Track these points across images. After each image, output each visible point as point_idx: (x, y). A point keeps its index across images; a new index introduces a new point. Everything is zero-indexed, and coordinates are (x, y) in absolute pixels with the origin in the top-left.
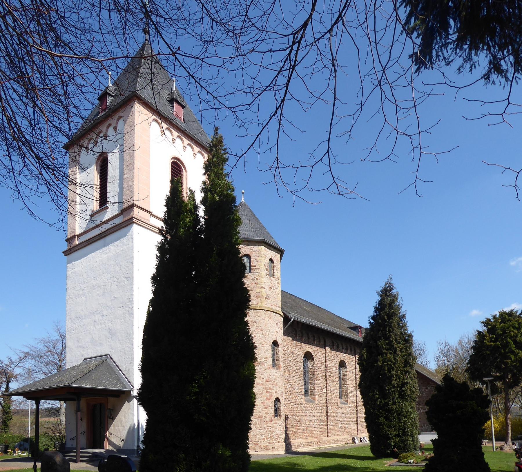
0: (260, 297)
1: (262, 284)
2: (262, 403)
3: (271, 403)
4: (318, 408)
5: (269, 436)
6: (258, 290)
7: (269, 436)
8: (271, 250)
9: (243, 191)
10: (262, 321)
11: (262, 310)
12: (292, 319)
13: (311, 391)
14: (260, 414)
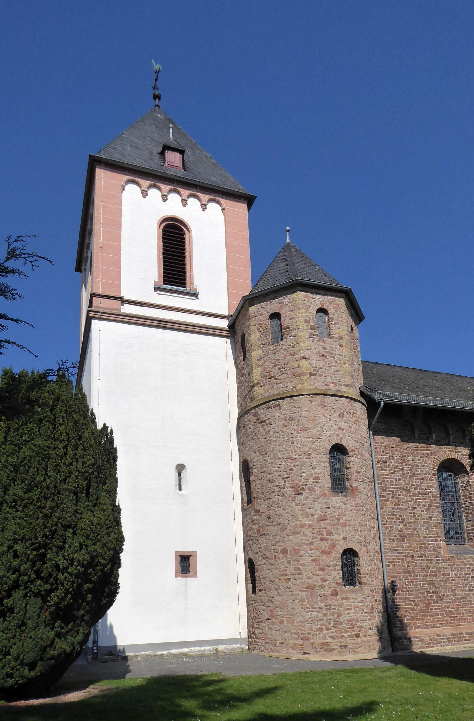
0: (299, 375)
1: (302, 352)
2: (313, 560)
3: (332, 559)
5: (332, 624)
6: (296, 364)
7: (332, 624)
8: (320, 294)
9: (288, 228)
10: (304, 414)
11: (303, 395)
12: (382, 403)
13: (469, 533)
14: (310, 581)
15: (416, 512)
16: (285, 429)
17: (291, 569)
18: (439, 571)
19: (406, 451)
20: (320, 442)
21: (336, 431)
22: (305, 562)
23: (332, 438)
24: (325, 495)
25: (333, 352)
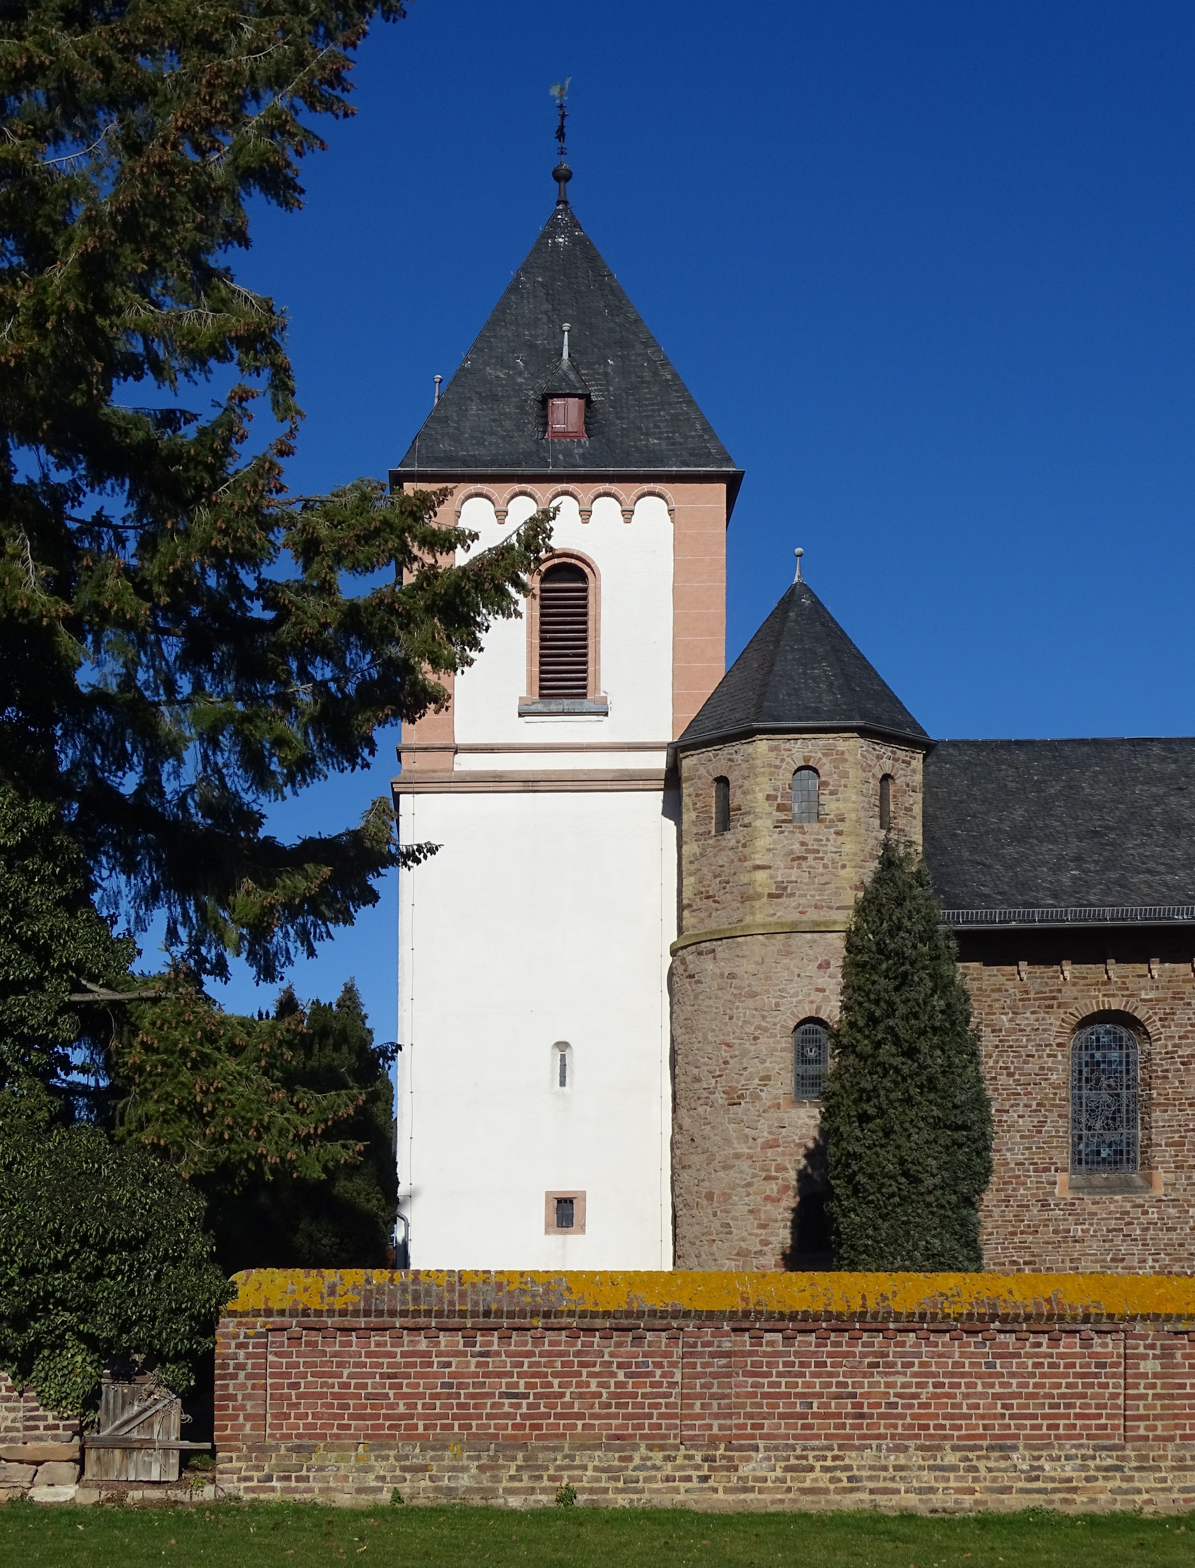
0: (750, 898)
3: (781, 1210)
4: (1172, 1211)
6: (744, 878)
9: (799, 550)
15: (1005, 1118)
16: (720, 993)
17: (716, 1225)
18: (1045, 1226)
20: (776, 1017)
21: (809, 995)
22: (738, 1214)
23: (800, 1008)
24: (778, 1106)
25: (821, 848)
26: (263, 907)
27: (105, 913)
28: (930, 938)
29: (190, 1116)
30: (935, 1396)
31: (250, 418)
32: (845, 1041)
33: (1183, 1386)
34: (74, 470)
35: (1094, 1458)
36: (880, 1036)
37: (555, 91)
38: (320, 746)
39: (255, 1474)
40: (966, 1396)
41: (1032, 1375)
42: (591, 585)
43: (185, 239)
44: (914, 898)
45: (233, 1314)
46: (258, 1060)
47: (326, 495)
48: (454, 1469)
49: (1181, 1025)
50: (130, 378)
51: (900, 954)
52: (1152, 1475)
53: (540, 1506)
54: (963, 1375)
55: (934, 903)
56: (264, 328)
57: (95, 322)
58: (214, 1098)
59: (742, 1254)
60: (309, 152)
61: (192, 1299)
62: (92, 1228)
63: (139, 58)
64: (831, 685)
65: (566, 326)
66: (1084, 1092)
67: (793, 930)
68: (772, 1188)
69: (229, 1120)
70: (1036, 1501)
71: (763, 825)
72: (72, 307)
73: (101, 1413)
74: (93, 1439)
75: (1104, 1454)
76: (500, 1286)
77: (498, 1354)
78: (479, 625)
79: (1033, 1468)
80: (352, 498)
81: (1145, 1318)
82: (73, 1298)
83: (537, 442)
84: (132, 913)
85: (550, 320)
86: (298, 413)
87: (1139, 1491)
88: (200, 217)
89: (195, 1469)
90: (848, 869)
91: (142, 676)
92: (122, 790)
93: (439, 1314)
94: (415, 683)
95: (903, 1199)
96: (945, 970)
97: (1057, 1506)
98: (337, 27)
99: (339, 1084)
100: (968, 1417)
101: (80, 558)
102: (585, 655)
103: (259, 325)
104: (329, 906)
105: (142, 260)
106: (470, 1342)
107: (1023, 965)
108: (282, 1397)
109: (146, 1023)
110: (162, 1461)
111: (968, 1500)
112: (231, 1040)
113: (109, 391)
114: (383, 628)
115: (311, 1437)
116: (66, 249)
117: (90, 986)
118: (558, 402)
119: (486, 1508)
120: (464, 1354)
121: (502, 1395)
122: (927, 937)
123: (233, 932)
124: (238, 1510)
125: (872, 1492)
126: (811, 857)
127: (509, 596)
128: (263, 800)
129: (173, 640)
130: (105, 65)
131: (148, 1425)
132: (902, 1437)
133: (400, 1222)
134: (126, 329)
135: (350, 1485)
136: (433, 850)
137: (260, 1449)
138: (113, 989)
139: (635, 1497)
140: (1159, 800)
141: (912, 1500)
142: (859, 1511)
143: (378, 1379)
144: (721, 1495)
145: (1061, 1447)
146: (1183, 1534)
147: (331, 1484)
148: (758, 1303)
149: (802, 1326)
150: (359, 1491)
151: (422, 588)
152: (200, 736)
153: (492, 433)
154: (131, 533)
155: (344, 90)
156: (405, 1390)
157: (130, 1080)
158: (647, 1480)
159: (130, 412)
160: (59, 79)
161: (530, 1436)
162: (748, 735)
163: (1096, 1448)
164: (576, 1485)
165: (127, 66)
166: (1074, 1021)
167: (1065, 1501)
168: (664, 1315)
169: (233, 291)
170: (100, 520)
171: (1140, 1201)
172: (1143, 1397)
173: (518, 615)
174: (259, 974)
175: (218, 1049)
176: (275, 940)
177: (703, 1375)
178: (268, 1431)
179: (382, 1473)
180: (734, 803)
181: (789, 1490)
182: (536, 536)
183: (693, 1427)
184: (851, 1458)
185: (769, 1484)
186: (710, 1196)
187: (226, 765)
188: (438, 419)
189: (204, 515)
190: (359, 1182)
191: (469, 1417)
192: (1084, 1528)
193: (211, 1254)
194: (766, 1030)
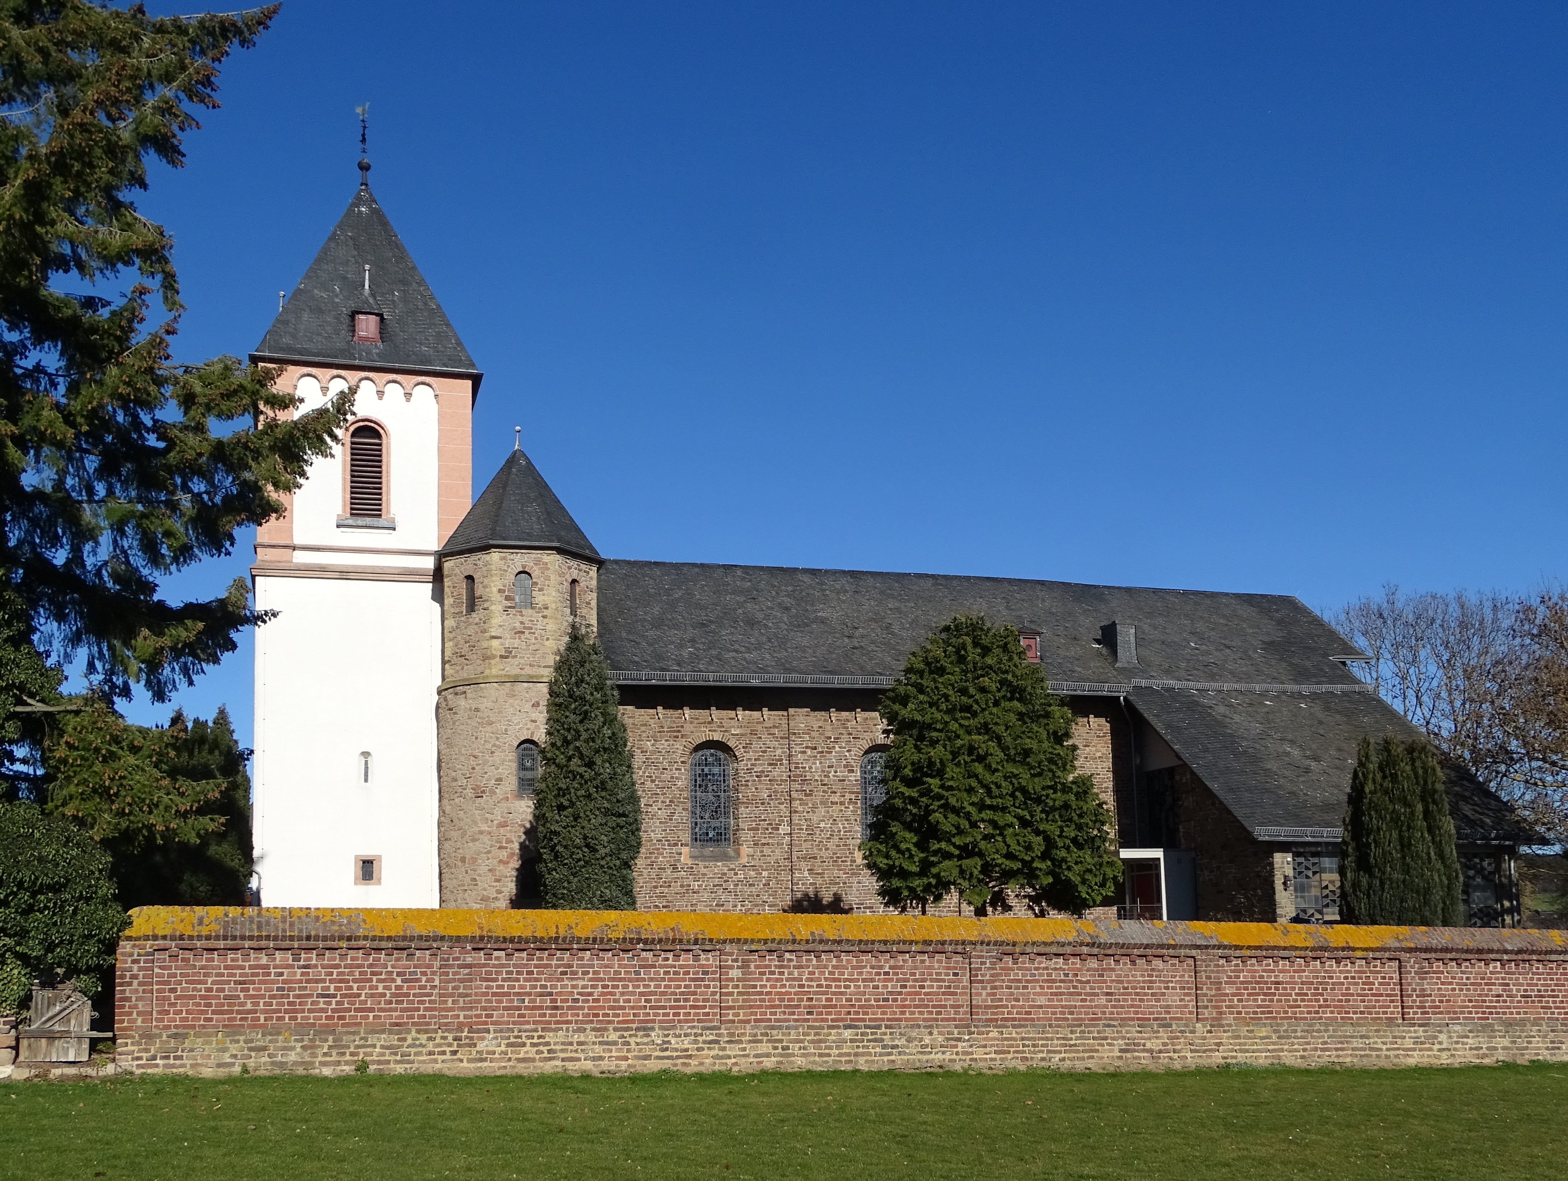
0: (488, 658)
4: (752, 873)
6: (485, 644)
9: (518, 428)
17: (468, 879)
19: (644, 735)
24: (507, 799)
26: (156, 649)
27: (42, 649)
28: (602, 689)
29: (101, 796)
30: (603, 994)
31: (147, 307)
32: (549, 755)
33: (755, 987)
34: (21, 332)
35: (702, 1035)
36: (571, 753)
37: (359, 110)
38: (197, 538)
39: (144, 1055)
40: (622, 994)
41: (663, 979)
42: (384, 441)
43: (101, 178)
44: (591, 662)
45: (129, 938)
46: (150, 757)
47: (200, 365)
48: (284, 1048)
49: (756, 752)
50: (61, 271)
51: (583, 698)
52: (737, 1046)
53: (344, 1073)
54: (620, 980)
55: (604, 665)
56: (157, 246)
57: (34, 230)
58: (118, 783)
59: (484, 899)
60: (188, 129)
61: (99, 928)
62: (26, 875)
63: (69, 50)
64: (539, 518)
65: (367, 267)
66: (698, 794)
67: (516, 681)
68: (504, 854)
69: (129, 800)
70: (666, 1064)
71: (497, 608)
72: (17, 216)
73: (31, 1012)
74: (26, 1031)
75: (708, 1032)
76: (317, 918)
77: (316, 966)
78: (306, 461)
79: (664, 1042)
80: (218, 367)
81: (732, 941)
82: (12, 927)
83: (348, 342)
84: (62, 650)
85: (357, 262)
86: (181, 306)
87: (729, 1057)
88: (111, 164)
89: (100, 1052)
90: (551, 641)
91: (69, 482)
92: (55, 562)
93: (276, 938)
94: (262, 498)
95: (586, 862)
96: (611, 709)
97: (679, 1067)
98: (208, 47)
99: (207, 774)
100: (623, 1008)
101: (24, 394)
102: (380, 489)
103: (154, 243)
104: (203, 651)
105: (69, 189)
106: (297, 959)
107: (660, 709)
108: (164, 999)
109: (70, 729)
110: (76, 1046)
111: (624, 1064)
112: (132, 742)
113: (46, 279)
114: (240, 459)
115: (185, 1027)
116: (16, 177)
117: (29, 701)
118: (362, 317)
119: (307, 1077)
120: (292, 967)
121: (319, 996)
122: (599, 688)
123: (134, 666)
124: (131, 1081)
125: (563, 1060)
126: (527, 632)
127: (326, 443)
128: (156, 573)
129: (93, 457)
130: (43, 52)
131: (66, 1020)
132: (582, 1022)
133: (255, 876)
134: (58, 237)
135: (212, 1062)
136: (275, 615)
137: (148, 1036)
138: (47, 704)
139: (408, 1066)
140: (741, 605)
141: (588, 1065)
142: (555, 1073)
143: (232, 985)
144: (465, 1064)
145: (682, 1028)
146: (756, 1085)
147: (199, 1061)
148: (489, 931)
149: (517, 946)
150: (219, 1065)
151: (267, 434)
152: (112, 526)
153: (319, 334)
154: (61, 379)
155: (212, 90)
156: (251, 992)
157: (58, 769)
158: (416, 1054)
159: (63, 296)
160: (11, 58)
161: (337, 1025)
162: (486, 548)
163: (703, 1028)
164: (369, 1058)
165: (60, 55)
166: (691, 747)
167: (684, 1064)
168: (428, 939)
169: (136, 219)
170: (38, 368)
171: (732, 866)
172: (731, 994)
173: (332, 456)
174: (154, 696)
175: (122, 748)
176: (165, 672)
177: (454, 980)
178: (154, 1023)
179: (235, 1052)
180: (478, 593)
181: (510, 1059)
182: (344, 404)
183: (446, 1017)
184: (550, 1037)
185: (497, 1056)
186: (463, 860)
187: (130, 548)
188: (282, 321)
189: (114, 371)
190: (225, 847)
191: (296, 1011)
192: (696, 1082)
193: (114, 895)
194: (499, 747)
